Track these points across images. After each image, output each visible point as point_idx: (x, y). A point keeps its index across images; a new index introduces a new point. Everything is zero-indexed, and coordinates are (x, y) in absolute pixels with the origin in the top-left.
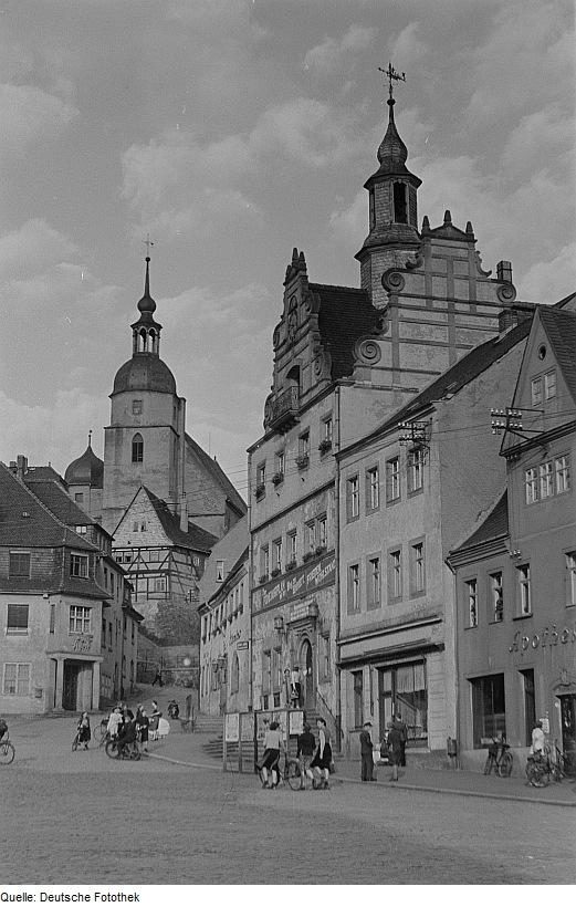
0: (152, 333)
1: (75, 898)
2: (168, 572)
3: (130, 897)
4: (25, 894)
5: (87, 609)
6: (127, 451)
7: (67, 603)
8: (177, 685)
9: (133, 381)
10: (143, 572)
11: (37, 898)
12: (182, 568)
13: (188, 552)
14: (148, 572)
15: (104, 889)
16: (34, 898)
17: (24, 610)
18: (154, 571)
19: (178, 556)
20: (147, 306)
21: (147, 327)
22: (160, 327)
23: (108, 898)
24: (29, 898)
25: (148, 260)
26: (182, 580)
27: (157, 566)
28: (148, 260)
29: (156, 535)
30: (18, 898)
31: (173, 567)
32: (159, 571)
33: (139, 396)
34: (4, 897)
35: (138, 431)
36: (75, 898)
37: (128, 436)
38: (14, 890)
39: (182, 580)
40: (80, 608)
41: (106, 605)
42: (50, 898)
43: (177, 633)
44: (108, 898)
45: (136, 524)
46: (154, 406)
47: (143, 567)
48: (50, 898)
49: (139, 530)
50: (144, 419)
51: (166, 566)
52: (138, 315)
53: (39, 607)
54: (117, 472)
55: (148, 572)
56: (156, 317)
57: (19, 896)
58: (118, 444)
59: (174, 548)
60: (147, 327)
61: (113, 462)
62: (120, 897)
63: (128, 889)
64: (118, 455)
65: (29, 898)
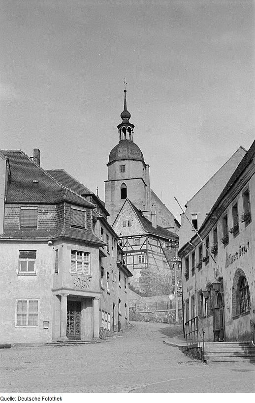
0: (129, 130)
1: (33, 399)
2: (146, 251)
3: (58, 398)
4: (11, 397)
5: (87, 254)
6: (118, 193)
7: (68, 248)
8: (156, 321)
9: (120, 155)
10: (130, 252)
11: (17, 399)
12: (154, 248)
13: (158, 238)
14: (133, 251)
15: (46, 395)
16: (15, 399)
17: (32, 255)
18: (137, 251)
19: (152, 241)
20: (125, 116)
21: (126, 126)
22: (133, 126)
23: (48, 399)
24: (13, 399)
25: (125, 91)
26: (155, 256)
27: (138, 248)
28: (125, 91)
29: (137, 228)
30: (8, 399)
31: (149, 248)
32: (141, 250)
33: (123, 163)
34: (2, 399)
35: (123, 182)
36: (33, 399)
37: (118, 186)
38: (6, 395)
39: (155, 256)
40: (80, 253)
41: (102, 255)
42: (22, 399)
43: (153, 289)
44: (48, 399)
45: (124, 222)
46: (134, 169)
47: (130, 249)
48: (22, 399)
49: (127, 225)
50: (126, 175)
51: (144, 248)
52: (121, 121)
53: (44, 251)
54: (113, 205)
55: (133, 251)
56: (131, 121)
57: (8, 398)
58: (113, 189)
59: (150, 236)
60: (126, 126)
61: (110, 200)
62: (54, 398)
63: (57, 395)
64: (113, 195)
65: (13, 399)
